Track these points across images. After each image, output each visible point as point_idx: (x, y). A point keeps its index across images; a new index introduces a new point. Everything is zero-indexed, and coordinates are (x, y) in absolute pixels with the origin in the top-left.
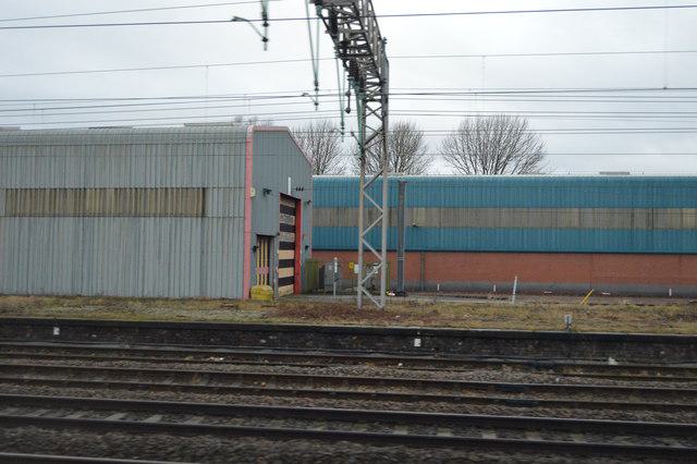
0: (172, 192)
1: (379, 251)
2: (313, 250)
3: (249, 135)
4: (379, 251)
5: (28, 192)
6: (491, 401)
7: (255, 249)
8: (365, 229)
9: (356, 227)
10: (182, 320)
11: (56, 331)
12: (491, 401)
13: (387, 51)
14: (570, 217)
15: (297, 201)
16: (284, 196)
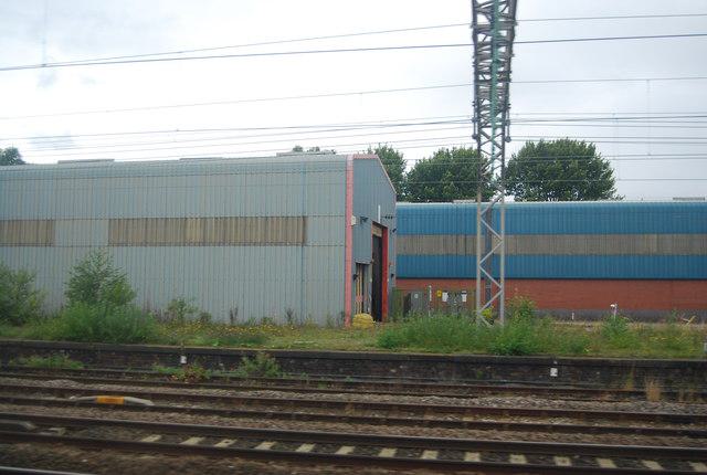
0: (272, 222)
1: (498, 279)
2: (397, 278)
3: (350, 164)
4: (498, 279)
5: (131, 222)
6: (633, 431)
7: (355, 277)
8: (483, 256)
9: (475, 256)
10: (308, 349)
11: (183, 360)
12: (633, 431)
13: (512, 66)
14: (650, 243)
15: (384, 229)
16: (375, 224)
